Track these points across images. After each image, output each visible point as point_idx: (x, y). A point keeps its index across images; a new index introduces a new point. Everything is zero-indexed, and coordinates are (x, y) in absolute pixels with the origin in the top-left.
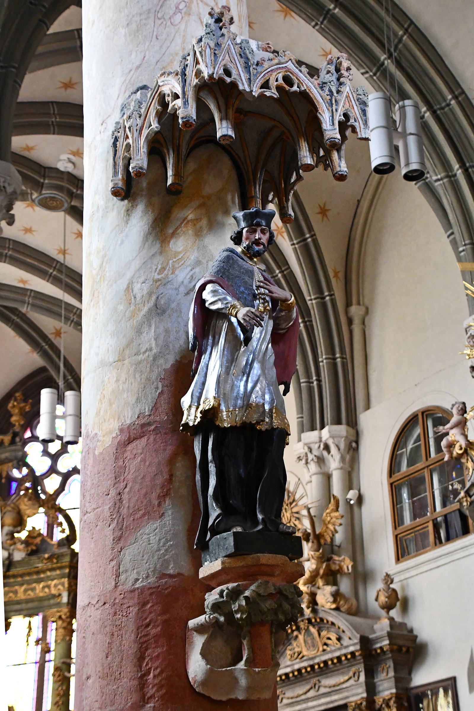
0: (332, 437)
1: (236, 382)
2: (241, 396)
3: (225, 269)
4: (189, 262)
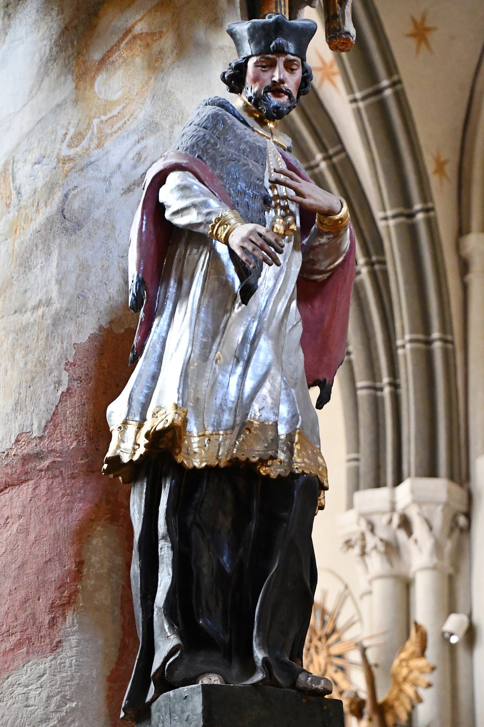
0: (418, 502)
1: (220, 377)
2: (230, 405)
3: (208, 142)
4: (132, 125)
